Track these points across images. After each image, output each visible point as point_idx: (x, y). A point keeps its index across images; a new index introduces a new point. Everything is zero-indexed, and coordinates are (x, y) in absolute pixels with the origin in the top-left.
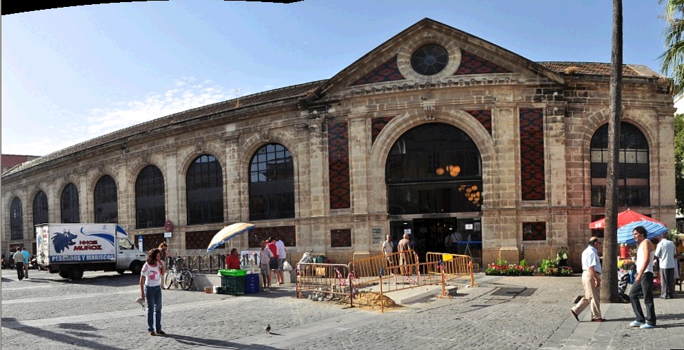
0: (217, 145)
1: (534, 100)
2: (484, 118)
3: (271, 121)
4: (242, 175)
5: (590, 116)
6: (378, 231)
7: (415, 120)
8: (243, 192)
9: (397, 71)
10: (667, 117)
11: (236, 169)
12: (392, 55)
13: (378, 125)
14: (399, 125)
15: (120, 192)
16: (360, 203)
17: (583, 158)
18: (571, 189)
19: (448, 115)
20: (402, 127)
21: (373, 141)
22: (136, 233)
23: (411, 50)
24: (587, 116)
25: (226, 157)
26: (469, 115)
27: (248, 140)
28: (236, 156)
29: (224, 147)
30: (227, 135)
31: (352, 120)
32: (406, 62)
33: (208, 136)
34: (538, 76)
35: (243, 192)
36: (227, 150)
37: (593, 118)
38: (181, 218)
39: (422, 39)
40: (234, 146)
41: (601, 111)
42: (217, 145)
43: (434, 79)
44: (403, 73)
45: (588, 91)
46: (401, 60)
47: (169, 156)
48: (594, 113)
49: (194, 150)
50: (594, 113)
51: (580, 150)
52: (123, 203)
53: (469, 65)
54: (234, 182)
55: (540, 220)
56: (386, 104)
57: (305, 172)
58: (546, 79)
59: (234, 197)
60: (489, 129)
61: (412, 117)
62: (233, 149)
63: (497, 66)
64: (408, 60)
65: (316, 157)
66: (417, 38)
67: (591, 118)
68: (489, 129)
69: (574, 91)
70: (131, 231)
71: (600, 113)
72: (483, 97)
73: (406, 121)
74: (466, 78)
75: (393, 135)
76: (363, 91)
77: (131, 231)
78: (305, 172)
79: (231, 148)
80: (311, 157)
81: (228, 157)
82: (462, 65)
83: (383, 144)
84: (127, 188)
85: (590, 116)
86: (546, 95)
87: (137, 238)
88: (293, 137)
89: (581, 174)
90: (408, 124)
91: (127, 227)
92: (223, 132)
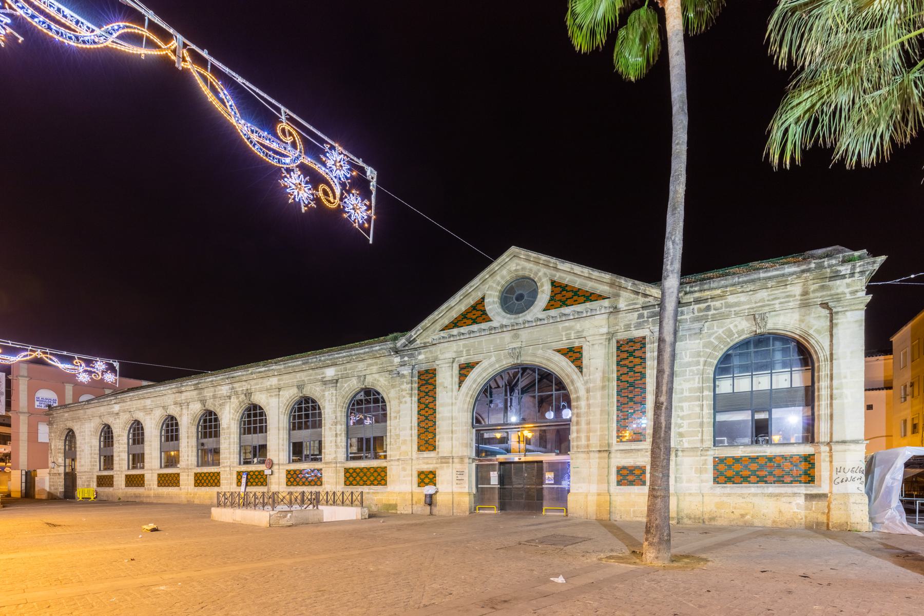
0: (318, 389)
1: (634, 327)
2: (574, 354)
3: (367, 367)
4: (339, 418)
5: (714, 336)
6: (462, 473)
7: (501, 364)
8: (340, 435)
9: (484, 312)
10: (848, 314)
11: (335, 412)
12: (480, 295)
13: (465, 369)
14: (485, 370)
15: (223, 429)
16: (444, 444)
17: (702, 390)
18: (682, 427)
19: (534, 355)
20: (488, 372)
21: (460, 386)
22: (238, 469)
23: (499, 288)
24: (710, 336)
25: (325, 400)
26: (558, 354)
27: (346, 385)
28: (334, 400)
29: (324, 391)
30: (326, 379)
31: (440, 366)
32: (494, 301)
33: (310, 379)
34: (640, 297)
35: (340, 435)
36: (326, 393)
37: (719, 338)
38: (281, 457)
39: (510, 272)
40: (333, 391)
41: (731, 326)
42: (318, 389)
43: (521, 318)
44: (490, 315)
45: (712, 304)
46: (489, 300)
47: (272, 396)
48: (720, 331)
49: (295, 392)
50: (720, 331)
51: (697, 380)
52: (225, 439)
53: (558, 297)
54: (332, 425)
55: (639, 464)
56: (472, 349)
57: (396, 417)
58: (650, 299)
59: (331, 439)
60: (580, 368)
61: (498, 360)
62: (332, 393)
63: (592, 294)
64: (496, 299)
65: (406, 402)
66: (504, 272)
67: (717, 338)
68: (580, 368)
69: (691, 307)
70: (234, 467)
71: (730, 331)
72: (573, 332)
73: (491, 365)
74: (553, 312)
75: (479, 380)
76: (451, 336)
77: (234, 467)
78: (396, 417)
79: (330, 392)
80: (401, 402)
81: (327, 401)
82: (552, 299)
83: (469, 389)
84: (230, 425)
85: (714, 336)
86: (650, 320)
87: (239, 474)
88: (386, 383)
89: (698, 410)
90: (494, 368)
91: (229, 463)
92: (323, 376)
